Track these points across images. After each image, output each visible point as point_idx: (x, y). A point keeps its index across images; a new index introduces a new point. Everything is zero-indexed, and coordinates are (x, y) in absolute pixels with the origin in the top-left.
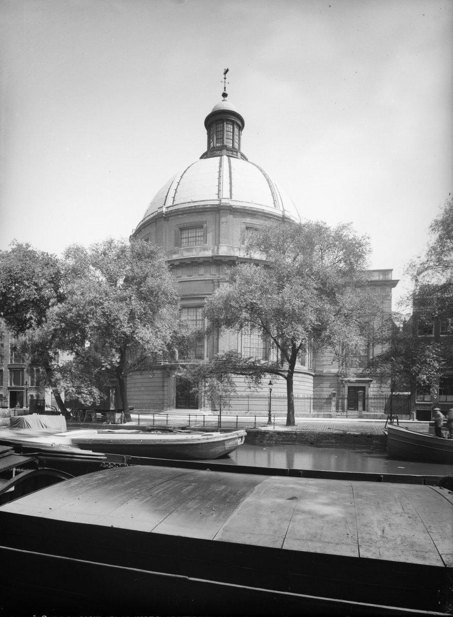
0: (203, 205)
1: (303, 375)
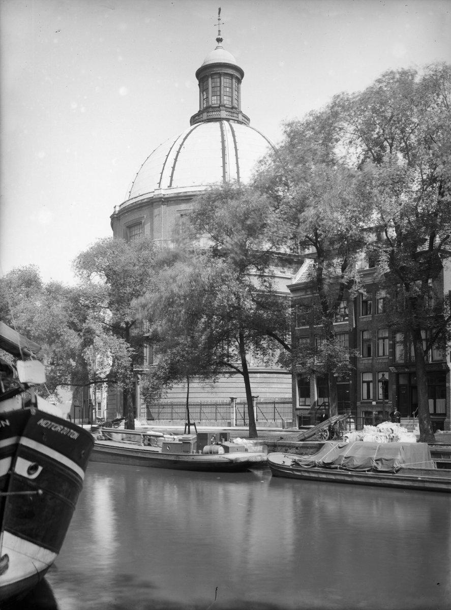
0: (142, 200)
1: (275, 375)
